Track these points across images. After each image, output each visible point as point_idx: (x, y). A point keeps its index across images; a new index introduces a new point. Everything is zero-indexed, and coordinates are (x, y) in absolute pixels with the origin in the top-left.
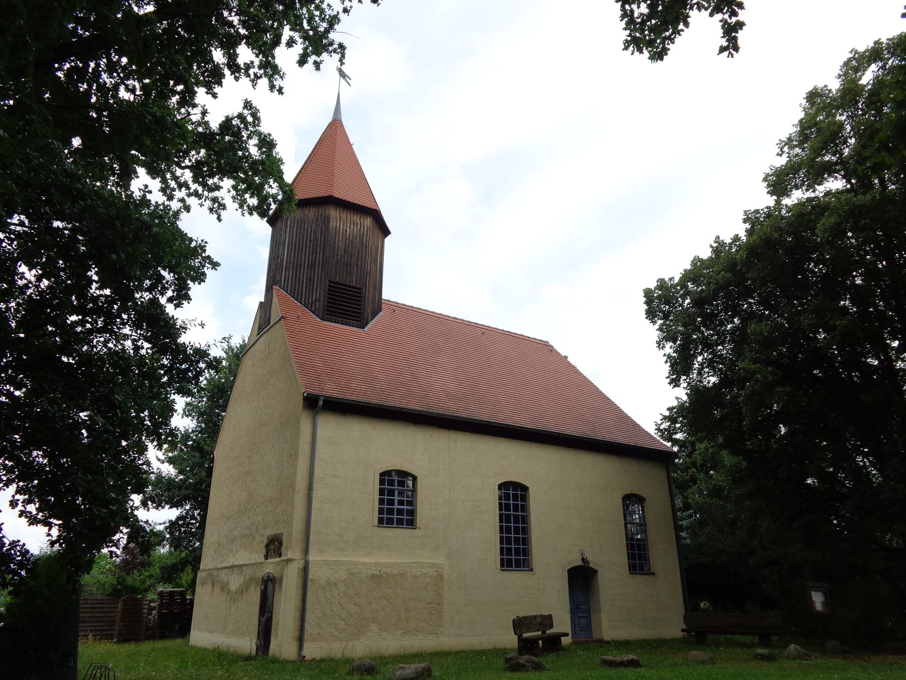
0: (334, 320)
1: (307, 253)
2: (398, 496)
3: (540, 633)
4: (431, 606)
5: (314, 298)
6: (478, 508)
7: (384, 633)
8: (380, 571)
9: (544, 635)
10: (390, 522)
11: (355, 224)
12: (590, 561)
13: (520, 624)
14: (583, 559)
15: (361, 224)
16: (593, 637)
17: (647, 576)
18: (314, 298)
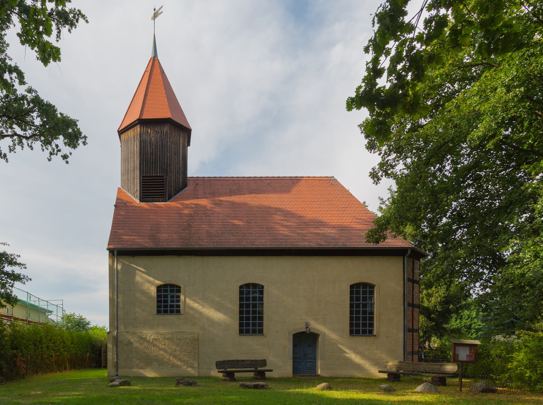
3: (254, 369)
15: (161, 131)
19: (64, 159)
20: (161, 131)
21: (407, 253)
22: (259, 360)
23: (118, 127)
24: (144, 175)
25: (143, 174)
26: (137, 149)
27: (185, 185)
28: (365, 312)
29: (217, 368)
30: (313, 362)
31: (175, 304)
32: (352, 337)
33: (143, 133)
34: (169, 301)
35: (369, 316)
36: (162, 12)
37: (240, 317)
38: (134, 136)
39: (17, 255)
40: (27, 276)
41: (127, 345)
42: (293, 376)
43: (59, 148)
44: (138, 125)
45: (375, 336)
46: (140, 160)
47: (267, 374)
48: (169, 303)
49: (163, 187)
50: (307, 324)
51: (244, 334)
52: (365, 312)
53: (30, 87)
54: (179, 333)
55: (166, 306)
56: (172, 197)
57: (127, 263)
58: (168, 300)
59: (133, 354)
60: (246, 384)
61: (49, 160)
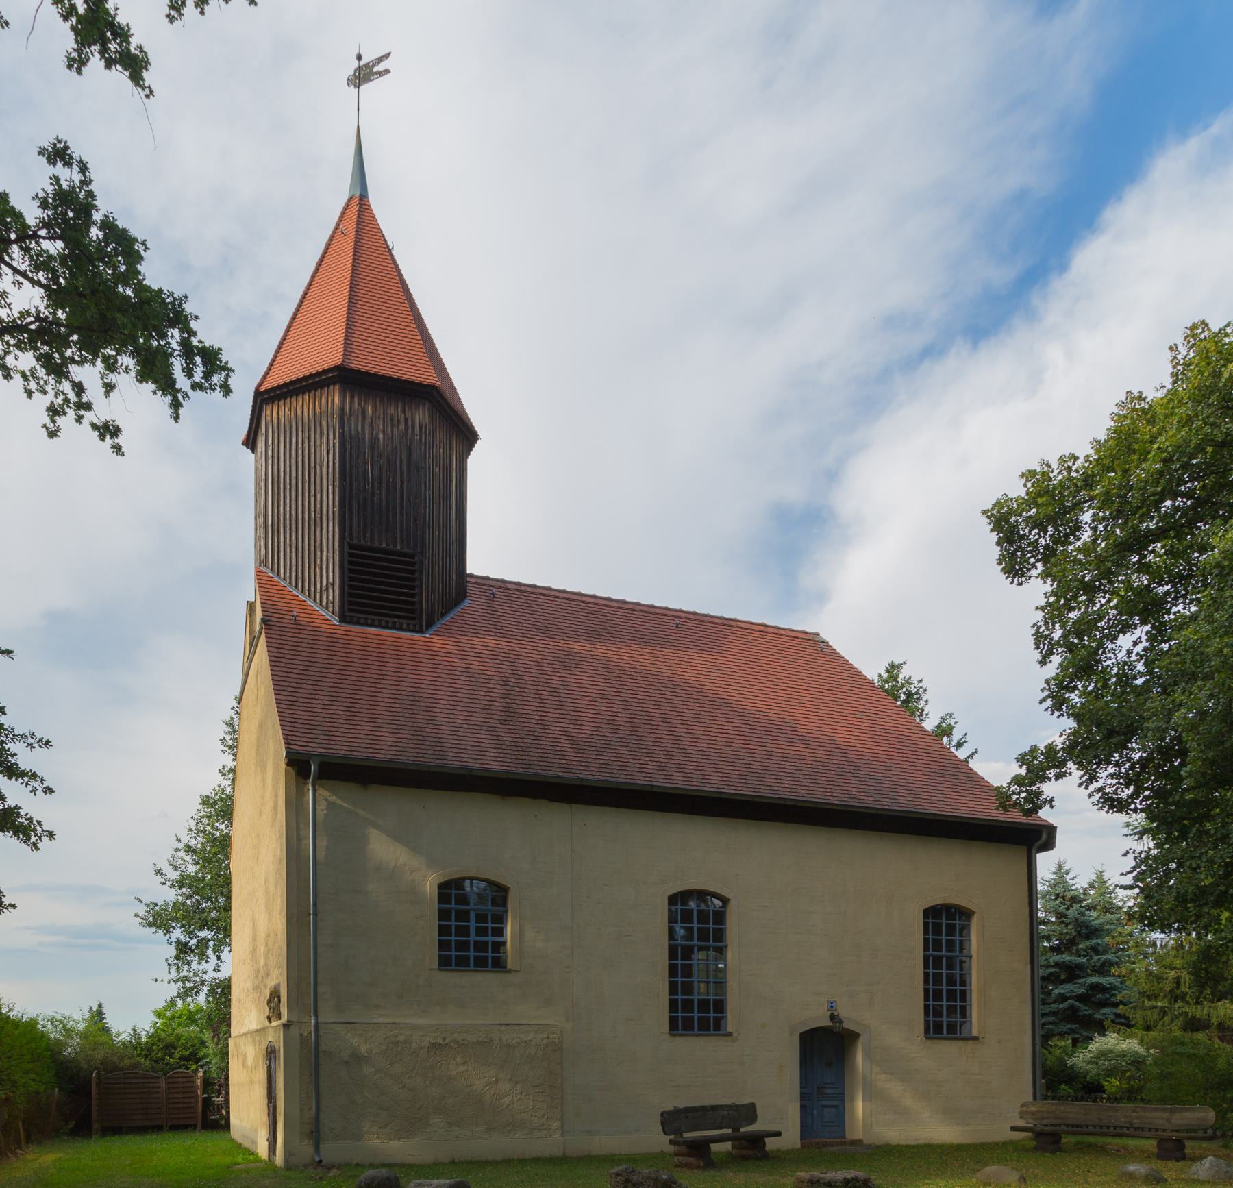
0: (362, 621)
1: (306, 495)
2: (477, 935)
3: (730, 1131)
4: (540, 1091)
5: (324, 583)
6: (627, 936)
7: (457, 1128)
8: (444, 1039)
9: (736, 1134)
10: (462, 963)
11: (395, 422)
12: (843, 1020)
13: (672, 1121)
14: (832, 1017)
15: (406, 420)
16: (847, 1136)
17: (961, 1043)
18: (324, 583)
19: (102, 437)
20: (406, 420)
21: (1040, 838)
22: (743, 1105)
23: (260, 377)
24: (355, 541)
25: (351, 539)
26: (330, 458)
27: (462, 595)
28: (951, 981)
29: (665, 1133)
30: (837, 1106)
31: (490, 939)
32: (929, 1042)
33: (350, 415)
34: (473, 931)
35: (933, 989)
36: (387, 71)
37: (670, 982)
38: (318, 420)
39: (41, 740)
40: (39, 823)
41: (347, 1063)
42: (803, 1146)
43: (85, 399)
44: (334, 384)
45: (976, 1038)
46: (340, 492)
47: (771, 1144)
48: (473, 937)
49: (413, 588)
50: (832, 1007)
51: (680, 1032)
52: (951, 981)
53: (60, 142)
54: (507, 1028)
55: (463, 946)
56: (434, 623)
57: (346, 805)
58: (469, 926)
59: (366, 1094)
60: (823, 1178)
61: (53, 434)
